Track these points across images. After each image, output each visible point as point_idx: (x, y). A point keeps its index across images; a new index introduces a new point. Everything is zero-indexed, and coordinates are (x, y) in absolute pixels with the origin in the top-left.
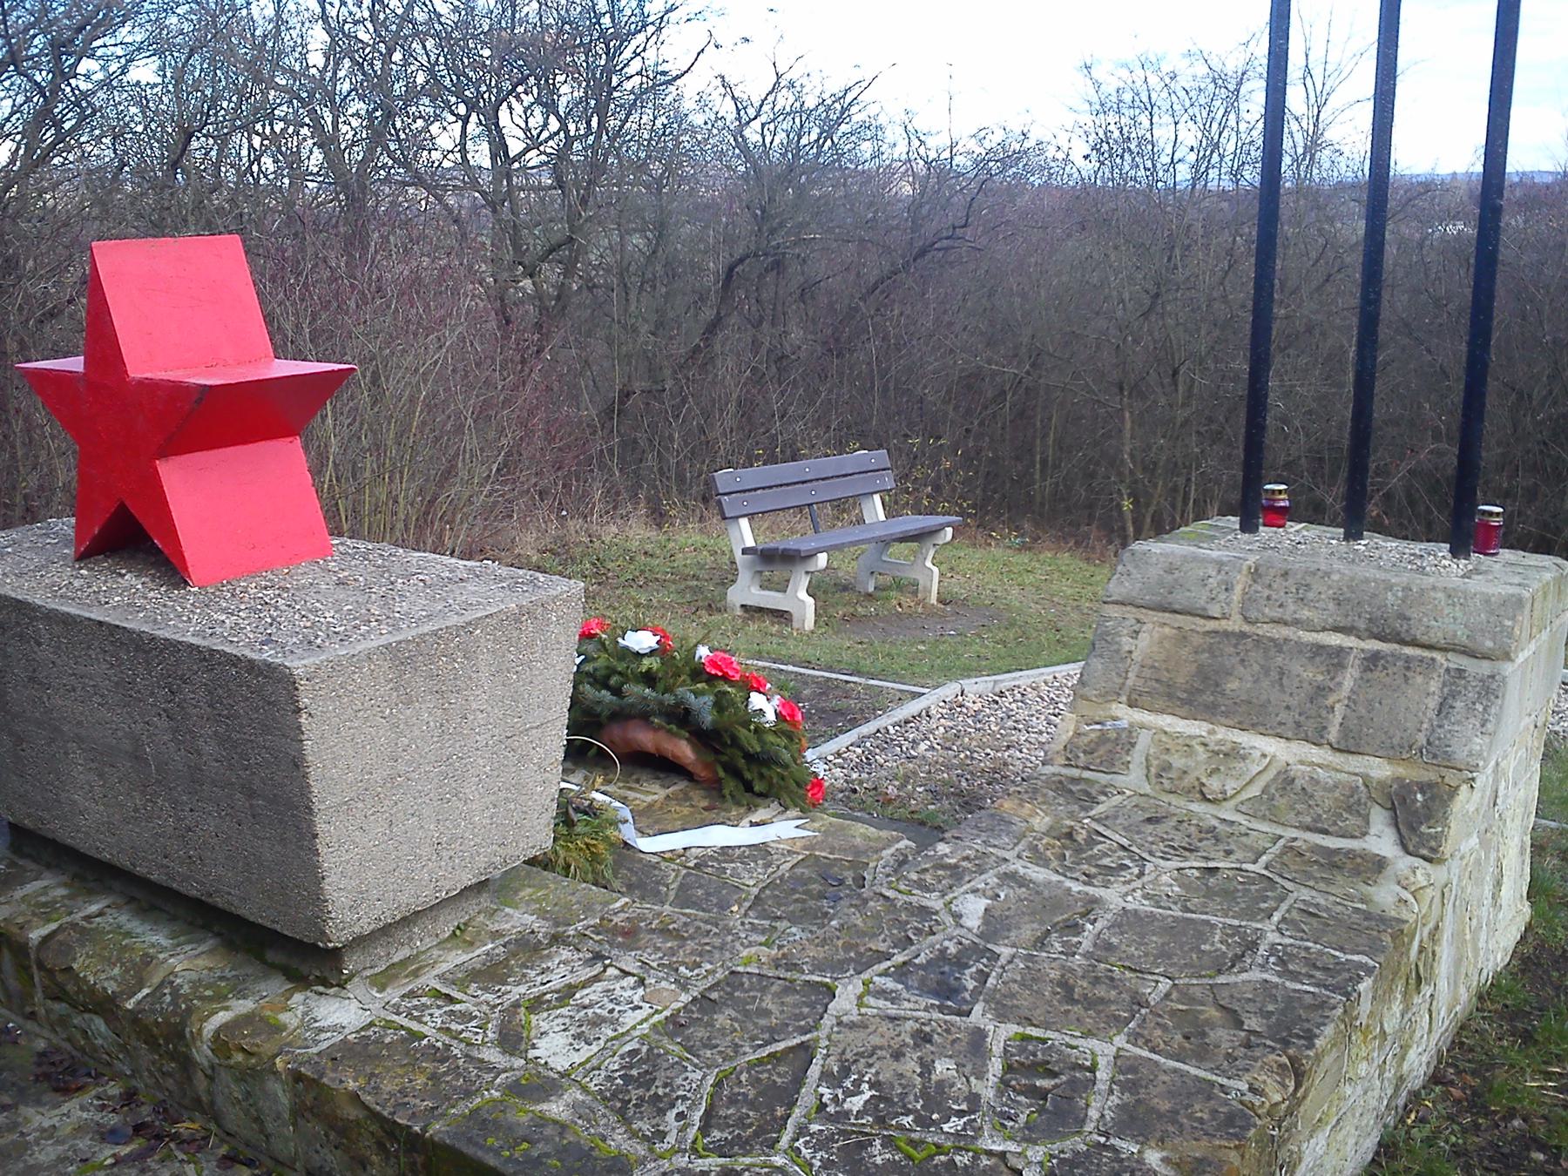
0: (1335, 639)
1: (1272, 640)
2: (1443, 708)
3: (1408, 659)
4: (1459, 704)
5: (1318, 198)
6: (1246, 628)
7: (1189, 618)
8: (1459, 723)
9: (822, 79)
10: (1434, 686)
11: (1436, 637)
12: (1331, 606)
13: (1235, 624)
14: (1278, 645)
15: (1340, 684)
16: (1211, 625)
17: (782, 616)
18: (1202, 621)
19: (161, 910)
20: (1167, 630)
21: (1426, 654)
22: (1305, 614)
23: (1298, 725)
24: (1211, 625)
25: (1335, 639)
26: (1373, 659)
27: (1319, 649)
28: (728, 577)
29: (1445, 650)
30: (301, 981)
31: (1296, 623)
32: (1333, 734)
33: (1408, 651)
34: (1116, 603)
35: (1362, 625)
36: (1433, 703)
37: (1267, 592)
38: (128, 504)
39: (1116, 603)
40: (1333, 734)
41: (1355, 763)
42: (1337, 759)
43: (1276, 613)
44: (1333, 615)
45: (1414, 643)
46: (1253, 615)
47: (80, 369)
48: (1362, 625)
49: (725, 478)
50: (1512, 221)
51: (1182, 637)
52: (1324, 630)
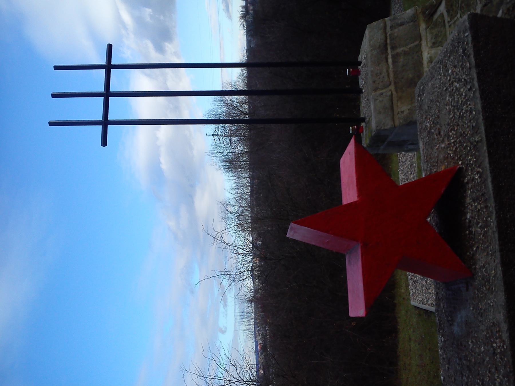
0: (390, 60)
1: (394, 75)
2: (402, 24)
3: (391, 40)
4: (400, 22)
5: (250, 78)
6: (393, 84)
7: (394, 106)
8: (405, 19)
10: (396, 30)
12: (381, 65)
13: (392, 87)
14: (395, 73)
15: (402, 51)
16: (394, 93)
18: (394, 96)
20: (399, 104)
21: (388, 37)
22: (385, 70)
23: (417, 52)
24: (394, 93)
25: (390, 60)
26: (393, 48)
27: (394, 62)
29: (386, 34)
31: (388, 71)
32: (417, 42)
33: (388, 41)
34: (394, 122)
35: (384, 56)
36: (401, 28)
39: (394, 122)
40: (417, 42)
41: (423, 32)
42: (423, 38)
43: (386, 78)
45: (386, 41)
48: (384, 56)
49: (359, 60)
50: (260, 87)
51: (400, 98)
52: (388, 64)
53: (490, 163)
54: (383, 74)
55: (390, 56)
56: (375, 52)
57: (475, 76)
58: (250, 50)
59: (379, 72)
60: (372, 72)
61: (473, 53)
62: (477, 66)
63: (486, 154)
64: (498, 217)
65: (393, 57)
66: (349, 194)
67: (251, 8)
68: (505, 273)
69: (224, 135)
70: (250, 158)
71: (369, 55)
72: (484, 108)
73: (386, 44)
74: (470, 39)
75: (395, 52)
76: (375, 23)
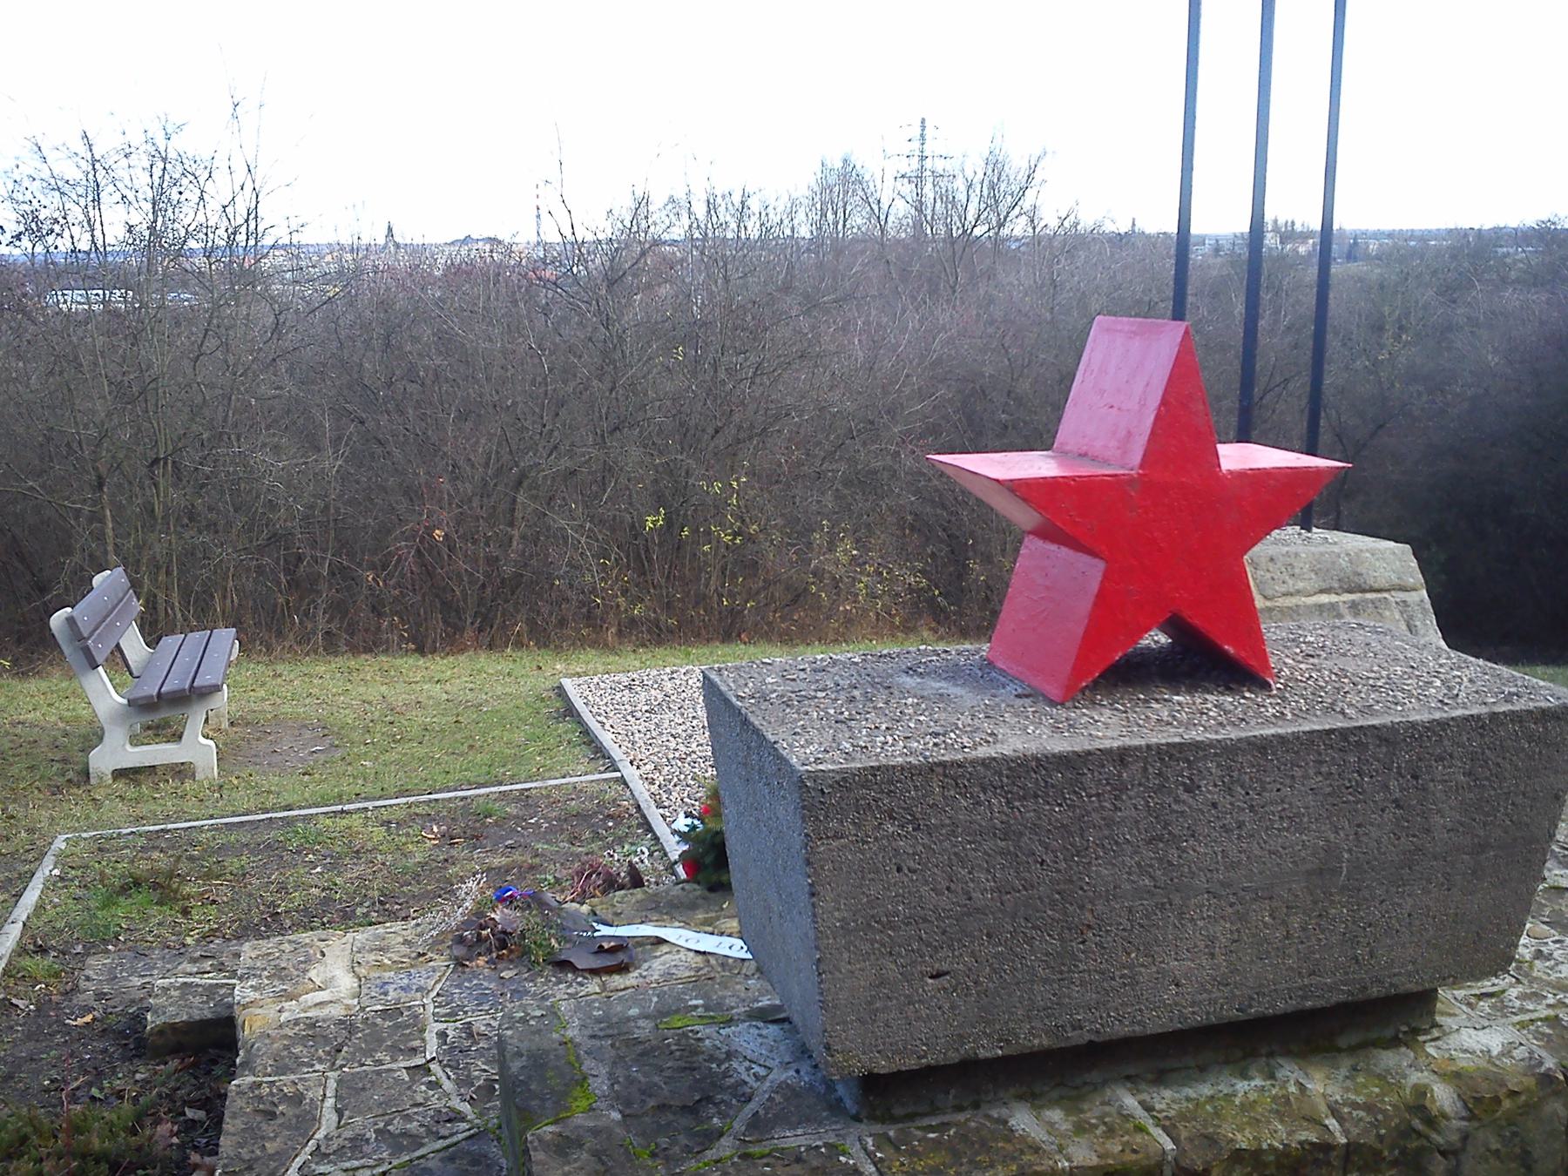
0: (1324, 599)
3: (1372, 602)
6: (1268, 604)
9: (962, 154)
11: (1382, 583)
17: (182, 771)
19: (1173, 1070)
22: (1300, 585)
25: (1324, 599)
26: (1354, 607)
28: (94, 736)
29: (1388, 590)
30: (1408, 1038)
33: (1369, 596)
35: (1336, 585)
36: (1404, 627)
37: (1268, 575)
38: (1187, 614)
43: (1283, 589)
44: (1315, 582)
46: (1269, 593)
47: (1224, 450)
53: (1312, 732)
54: (1291, 582)
55: (1333, 598)
56: (1343, 562)
57: (1474, 711)
58: (1355, 248)
59: (1297, 571)
60: (1297, 555)
61: (1517, 708)
62: (1494, 716)
63: (1327, 727)
64: (1211, 744)
65: (1333, 607)
66: (1235, 457)
67: (1302, 250)
68: (1106, 752)
69: (923, 158)
70: (864, 240)
71: (1336, 549)
72: (1413, 725)
73: (1364, 591)
74: (1543, 704)
75: (1344, 610)
76: (1414, 564)
